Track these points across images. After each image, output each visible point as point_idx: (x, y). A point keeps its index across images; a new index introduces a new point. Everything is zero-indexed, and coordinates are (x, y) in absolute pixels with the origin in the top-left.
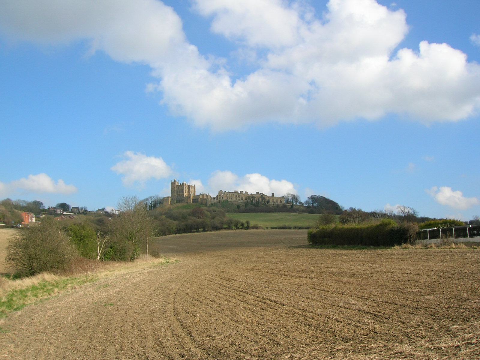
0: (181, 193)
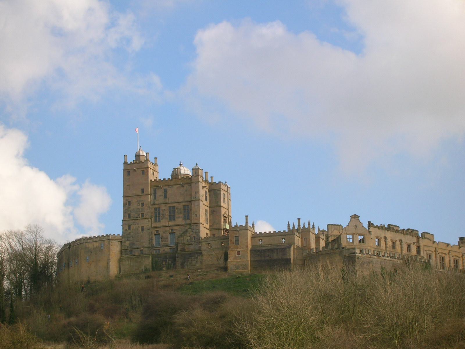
0: (180, 220)
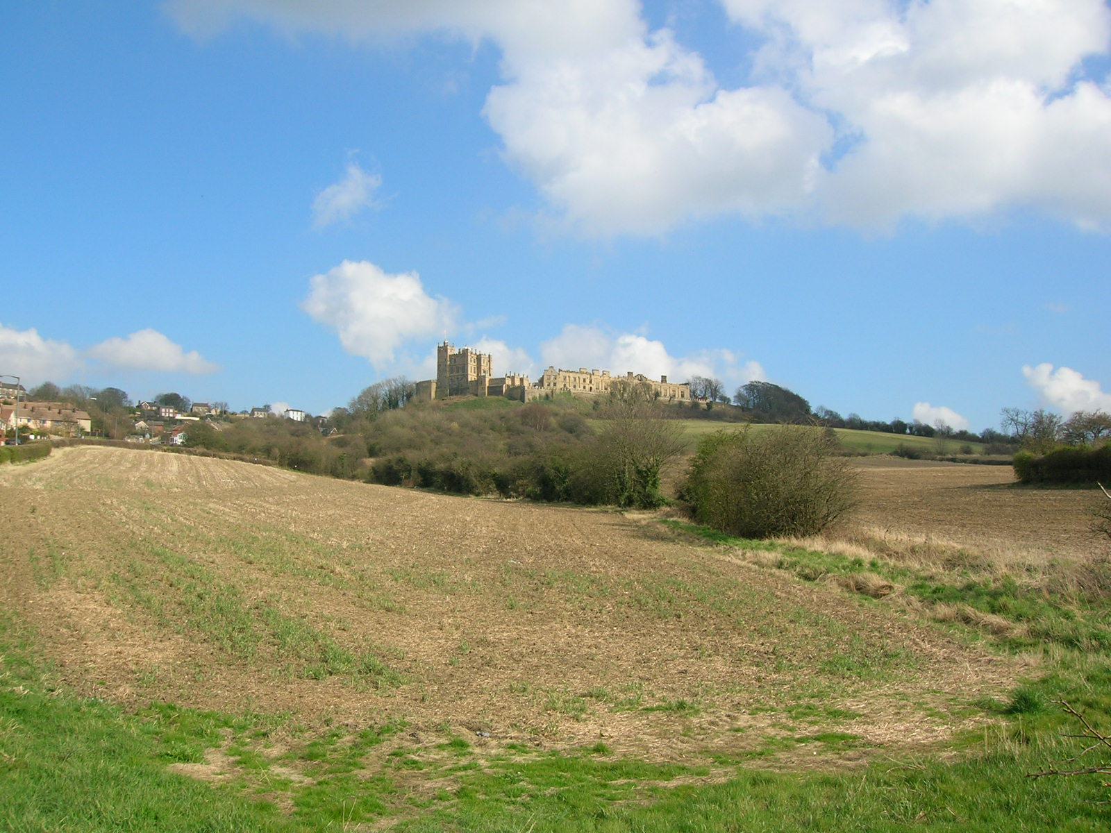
0: (460, 373)
